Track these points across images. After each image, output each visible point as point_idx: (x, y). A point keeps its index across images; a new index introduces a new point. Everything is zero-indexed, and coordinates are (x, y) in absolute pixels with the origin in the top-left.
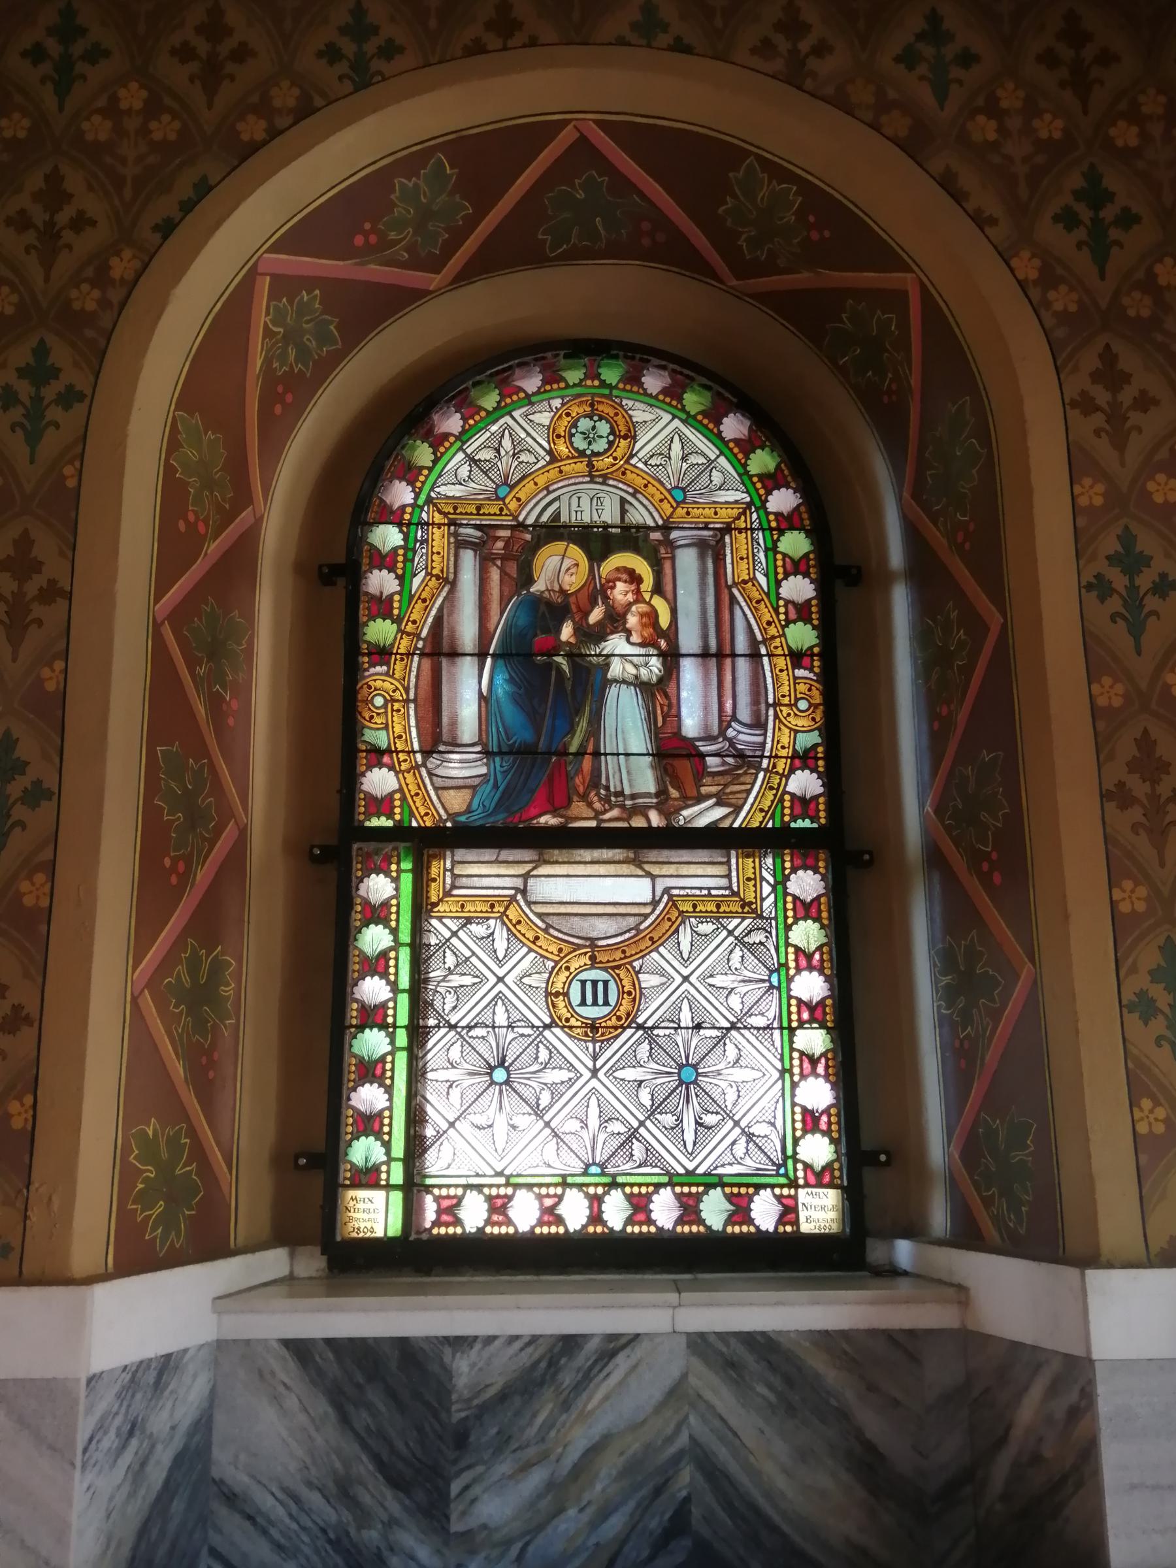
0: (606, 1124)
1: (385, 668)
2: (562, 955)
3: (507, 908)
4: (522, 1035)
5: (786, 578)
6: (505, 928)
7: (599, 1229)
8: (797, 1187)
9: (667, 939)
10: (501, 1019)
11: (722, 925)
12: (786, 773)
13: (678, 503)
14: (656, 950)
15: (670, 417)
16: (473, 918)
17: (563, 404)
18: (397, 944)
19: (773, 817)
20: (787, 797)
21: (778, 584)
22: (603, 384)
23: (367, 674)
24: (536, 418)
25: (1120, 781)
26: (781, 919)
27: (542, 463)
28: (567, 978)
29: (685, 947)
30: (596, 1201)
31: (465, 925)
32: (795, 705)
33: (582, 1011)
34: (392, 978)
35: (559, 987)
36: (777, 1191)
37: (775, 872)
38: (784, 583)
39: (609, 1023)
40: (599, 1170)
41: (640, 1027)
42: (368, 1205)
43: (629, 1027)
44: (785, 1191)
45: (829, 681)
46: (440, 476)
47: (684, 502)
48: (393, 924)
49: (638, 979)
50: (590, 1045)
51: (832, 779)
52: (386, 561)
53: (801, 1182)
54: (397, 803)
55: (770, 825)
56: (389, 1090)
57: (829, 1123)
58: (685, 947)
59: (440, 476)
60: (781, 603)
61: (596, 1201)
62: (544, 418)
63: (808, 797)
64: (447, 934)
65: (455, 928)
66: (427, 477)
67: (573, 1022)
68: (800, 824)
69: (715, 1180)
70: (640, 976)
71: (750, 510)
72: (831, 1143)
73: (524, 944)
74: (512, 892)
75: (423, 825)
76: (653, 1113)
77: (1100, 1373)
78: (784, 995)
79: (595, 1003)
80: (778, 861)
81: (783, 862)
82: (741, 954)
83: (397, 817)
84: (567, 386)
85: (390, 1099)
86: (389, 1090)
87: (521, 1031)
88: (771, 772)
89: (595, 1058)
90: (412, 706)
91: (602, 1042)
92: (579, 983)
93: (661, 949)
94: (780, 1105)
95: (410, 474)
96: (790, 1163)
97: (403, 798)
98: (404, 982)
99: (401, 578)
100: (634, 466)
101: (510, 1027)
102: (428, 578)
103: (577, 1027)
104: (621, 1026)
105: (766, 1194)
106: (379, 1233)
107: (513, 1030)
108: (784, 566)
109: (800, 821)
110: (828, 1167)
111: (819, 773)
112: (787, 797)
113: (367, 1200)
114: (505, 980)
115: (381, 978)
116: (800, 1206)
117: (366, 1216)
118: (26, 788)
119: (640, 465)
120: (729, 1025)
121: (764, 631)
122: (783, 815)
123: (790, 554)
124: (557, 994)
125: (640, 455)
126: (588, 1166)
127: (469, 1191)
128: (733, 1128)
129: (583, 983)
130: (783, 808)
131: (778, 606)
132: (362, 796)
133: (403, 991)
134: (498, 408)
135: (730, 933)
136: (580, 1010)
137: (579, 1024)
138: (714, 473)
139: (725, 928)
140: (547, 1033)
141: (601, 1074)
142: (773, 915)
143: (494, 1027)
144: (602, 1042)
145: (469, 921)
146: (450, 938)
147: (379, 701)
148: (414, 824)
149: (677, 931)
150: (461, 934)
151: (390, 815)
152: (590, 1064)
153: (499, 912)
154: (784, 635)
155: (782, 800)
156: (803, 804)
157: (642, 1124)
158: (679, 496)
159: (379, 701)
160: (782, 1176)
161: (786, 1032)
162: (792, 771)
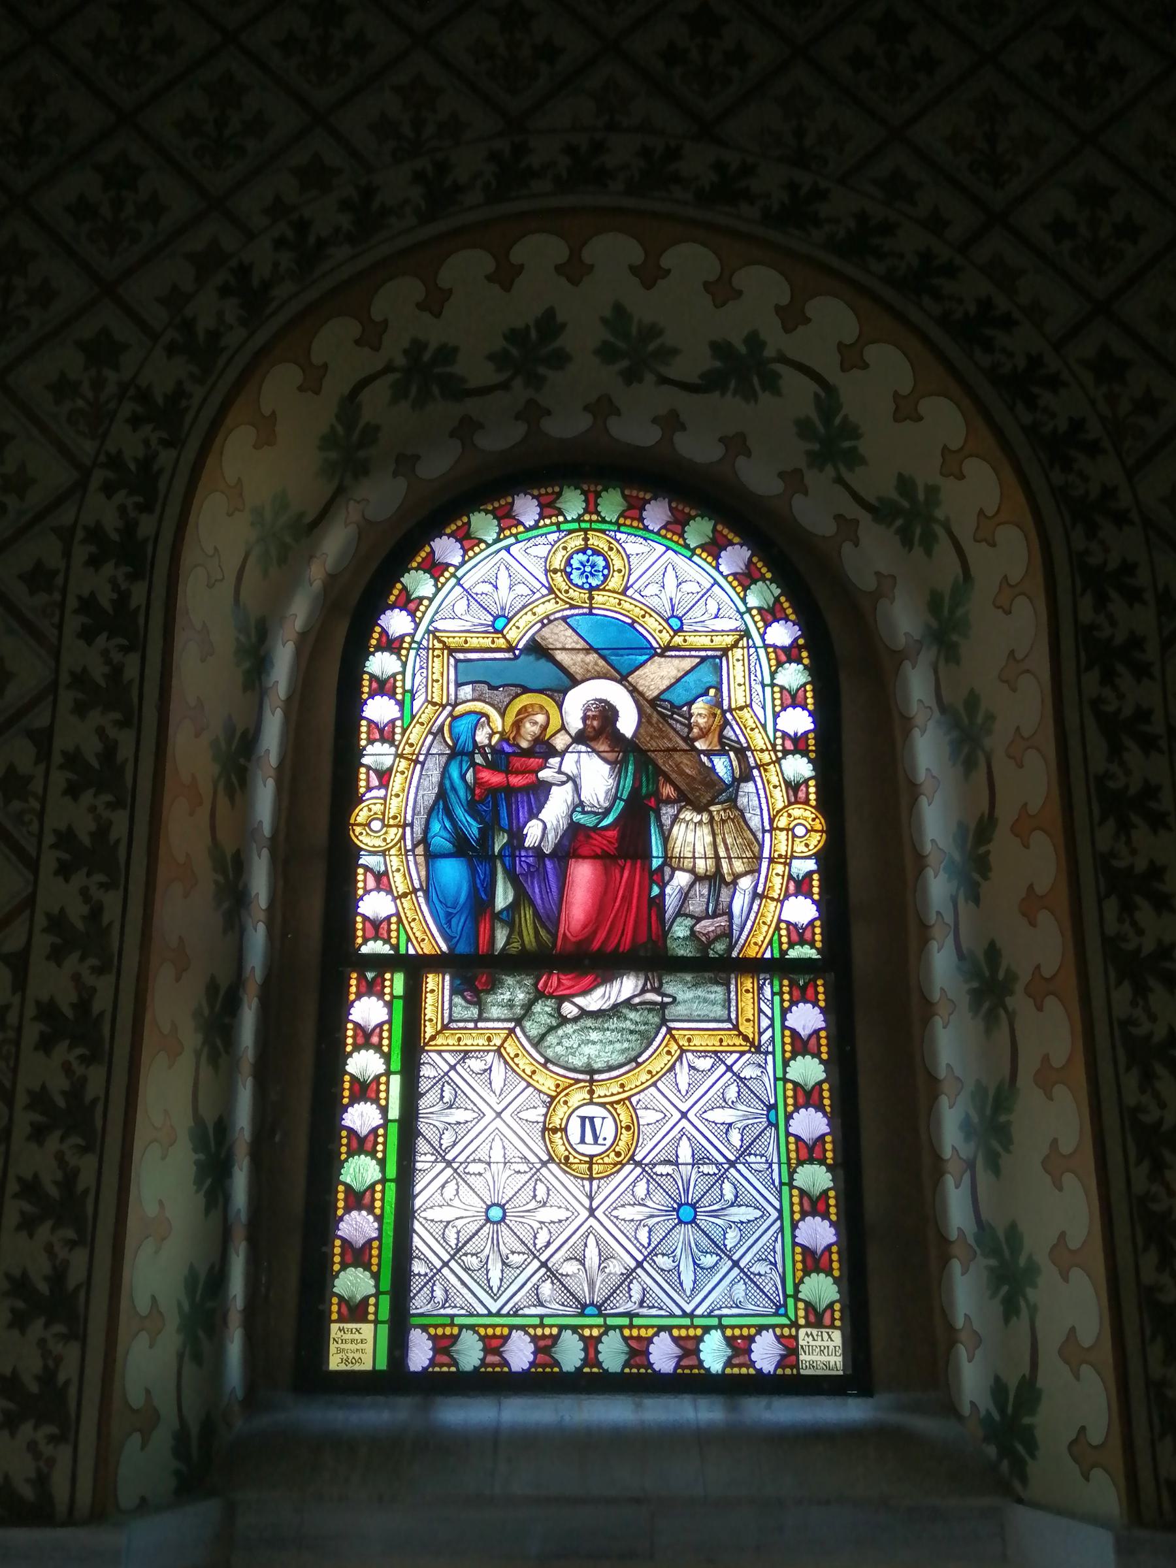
3: (505, 1040)
4: (519, 1172)
5: (802, 1219)
10: (497, 1155)
11: (720, 1059)
12: (781, 898)
16: (471, 1051)
18: (388, 1073)
20: (783, 925)
27: (538, 595)
34: (383, 1102)
35: (556, 1122)
37: (772, 1004)
41: (638, 1164)
42: (357, 1336)
43: (628, 1163)
47: (681, 629)
48: (375, 1268)
50: (587, 1183)
54: (394, 927)
55: (768, 955)
60: (779, 734)
62: (543, 551)
64: (446, 1068)
66: (427, 607)
69: (715, 1322)
73: (523, 1079)
75: (420, 952)
91: (599, 1179)
92: (579, 1120)
95: (409, 604)
96: (791, 1301)
98: (394, 1113)
99: (401, 704)
100: (631, 597)
104: (620, 1163)
106: (367, 1366)
108: (789, 936)
111: (820, 1008)
112: (783, 925)
113: (354, 1330)
115: (365, 1270)
117: (354, 1347)
119: (637, 596)
123: (787, 687)
124: (555, 1131)
125: (636, 586)
129: (583, 1119)
132: (344, 1133)
133: (390, 1181)
139: (724, 1063)
143: (489, 1164)
145: (466, 1054)
146: (449, 1071)
148: (411, 951)
149: (672, 1068)
152: (586, 1202)
153: (495, 1045)
154: (782, 903)
156: (799, 934)
158: (675, 623)
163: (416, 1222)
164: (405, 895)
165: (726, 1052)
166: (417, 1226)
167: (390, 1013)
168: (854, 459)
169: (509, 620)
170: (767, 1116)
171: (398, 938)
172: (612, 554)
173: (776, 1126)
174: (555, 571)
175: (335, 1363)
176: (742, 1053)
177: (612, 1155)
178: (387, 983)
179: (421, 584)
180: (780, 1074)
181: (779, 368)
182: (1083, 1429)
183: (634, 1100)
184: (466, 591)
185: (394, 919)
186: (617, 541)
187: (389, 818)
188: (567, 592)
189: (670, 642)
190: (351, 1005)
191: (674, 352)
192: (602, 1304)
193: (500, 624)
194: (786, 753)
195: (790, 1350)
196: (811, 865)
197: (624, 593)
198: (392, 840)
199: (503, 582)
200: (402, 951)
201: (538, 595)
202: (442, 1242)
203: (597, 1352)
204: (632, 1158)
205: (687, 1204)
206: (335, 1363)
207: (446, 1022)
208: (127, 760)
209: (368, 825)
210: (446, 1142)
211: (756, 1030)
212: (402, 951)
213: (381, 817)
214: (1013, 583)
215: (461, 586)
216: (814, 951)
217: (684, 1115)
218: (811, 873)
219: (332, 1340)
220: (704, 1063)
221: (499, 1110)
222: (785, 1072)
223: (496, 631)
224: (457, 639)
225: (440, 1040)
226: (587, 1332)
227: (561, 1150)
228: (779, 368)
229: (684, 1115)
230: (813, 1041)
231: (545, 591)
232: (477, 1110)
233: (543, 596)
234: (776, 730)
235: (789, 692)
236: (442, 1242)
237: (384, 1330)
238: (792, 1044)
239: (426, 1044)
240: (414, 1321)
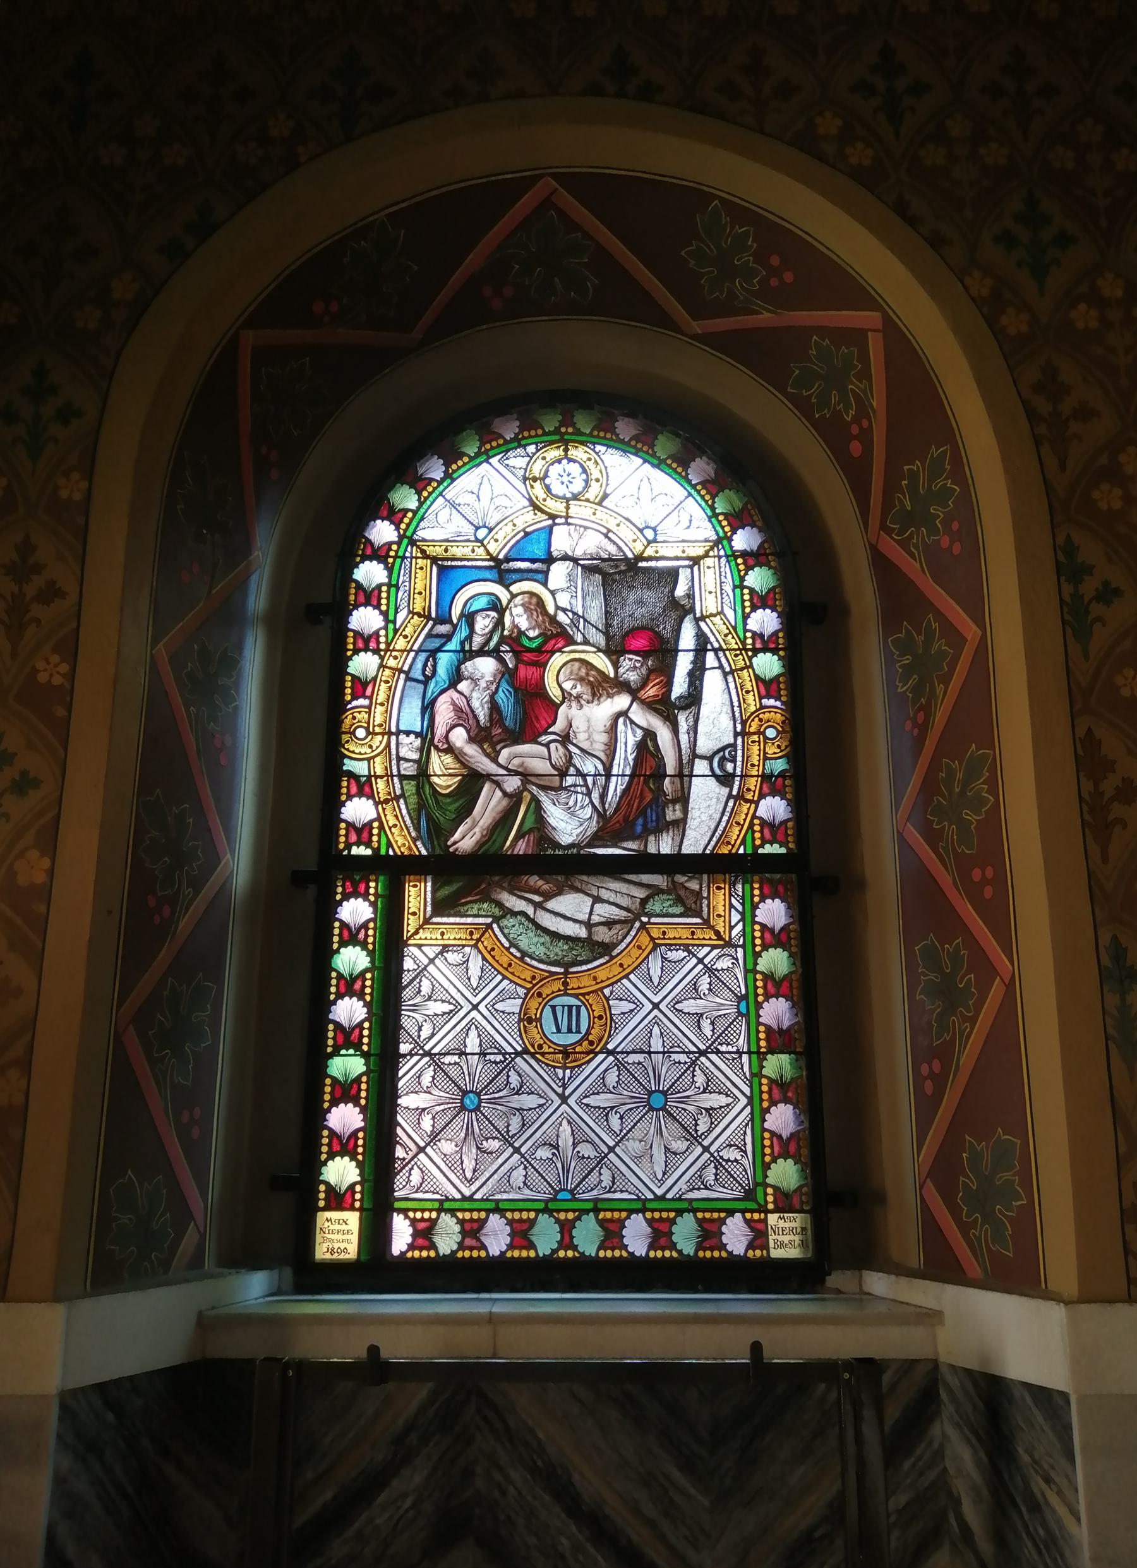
0: (458, 1149)
2: (534, 982)
6: (480, 956)
7: (570, 1254)
9: (493, 967)
13: (649, 542)
14: (627, 977)
21: (746, 617)
23: (349, 706)
24: (511, 462)
25: (1130, 805)
28: (540, 1004)
29: (655, 973)
30: (566, 1228)
36: (748, 1215)
40: (569, 1197)
43: (601, 1052)
44: (756, 1216)
47: (655, 541)
49: (608, 1004)
51: (798, 805)
52: (370, 597)
53: (771, 1206)
54: (375, 831)
55: (741, 851)
57: (799, 1147)
58: (655, 973)
60: (749, 635)
61: (566, 1228)
63: (777, 822)
67: (545, 1049)
68: (768, 849)
69: (685, 1205)
71: (718, 548)
72: (357, 1166)
74: (489, 920)
77: (72, 1385)
79: (570, 1031)
80: (747, 887)
81: (752, 889)
82: (708, 980)
84: (545, 434)
87: (492, 1058)
91: (573, 1068)
93: (632, 977)
94: (749, 1131)
97: (381, 827)
99: (385, 614)
101: (482, 1054)
102: (411, 615)
103: (549, 1053)
104: (592, 1051)
107: (738, 1050)
109: (767, 846)
113: (341, 1221)
114: (471, 1007)
117: (340, 1237)
118: (1118, 786)
126: (557, 1192)
127: (541, 1214)
128: (512, 1155)
130: (754, 832)
131: (745, 638)
134: (478, 455)
135: (700, 961)
137: (551, 1050)
139: (694, 955)
140: (518, 1060)
141: (571, 1101)
142: (741, 942)
143: (649, 1053)
144: (573, 1068)
151: (368, 844)
154: (751, 666)
156: (772, 830)
157: (706, 1149)
158: (649, 534)
161: (754, 1057)
163: (398, 1116)
164: (386, 801)
165: (698, 946)
166: (399, 1118)
169: (491, 530)
170: (738, 1006)
171: (379, 842)
172: (591, 464)
175: (322, 1253)
177: (585, 1043)
179: (405, 498)
180: (750, 966)
183: (607, 992)
184: (449, 501)
187: (374, 726)
189: (644, 551)
190: (343, 804)
193: (481, 533)
194: (756, 652)
197: (600, 504)
198: (377, 747)
199: (485, 494)
200: (383, 852)
202: (435, 982)
203: (572, 1237)
205: (658, 1091)
206: (322, 1253)
207: (428, 915)
209: (353, 733)
210: (425, 1033)
211: (727, 924)
213: (366, 725)
215: (444, 497)
217: (656, 1006)
219: (318, 1230)
221: (475, 1003)
222: (756, 964)
223: (477, 540)
224: (437, 548)
225: (421, 934)
226: (562, 1216)
229: (656, 1006)
232: (454, 1002)
234: (745, 631)
236: (435, 982)
239: (408, 939)
240: (397, 1205)
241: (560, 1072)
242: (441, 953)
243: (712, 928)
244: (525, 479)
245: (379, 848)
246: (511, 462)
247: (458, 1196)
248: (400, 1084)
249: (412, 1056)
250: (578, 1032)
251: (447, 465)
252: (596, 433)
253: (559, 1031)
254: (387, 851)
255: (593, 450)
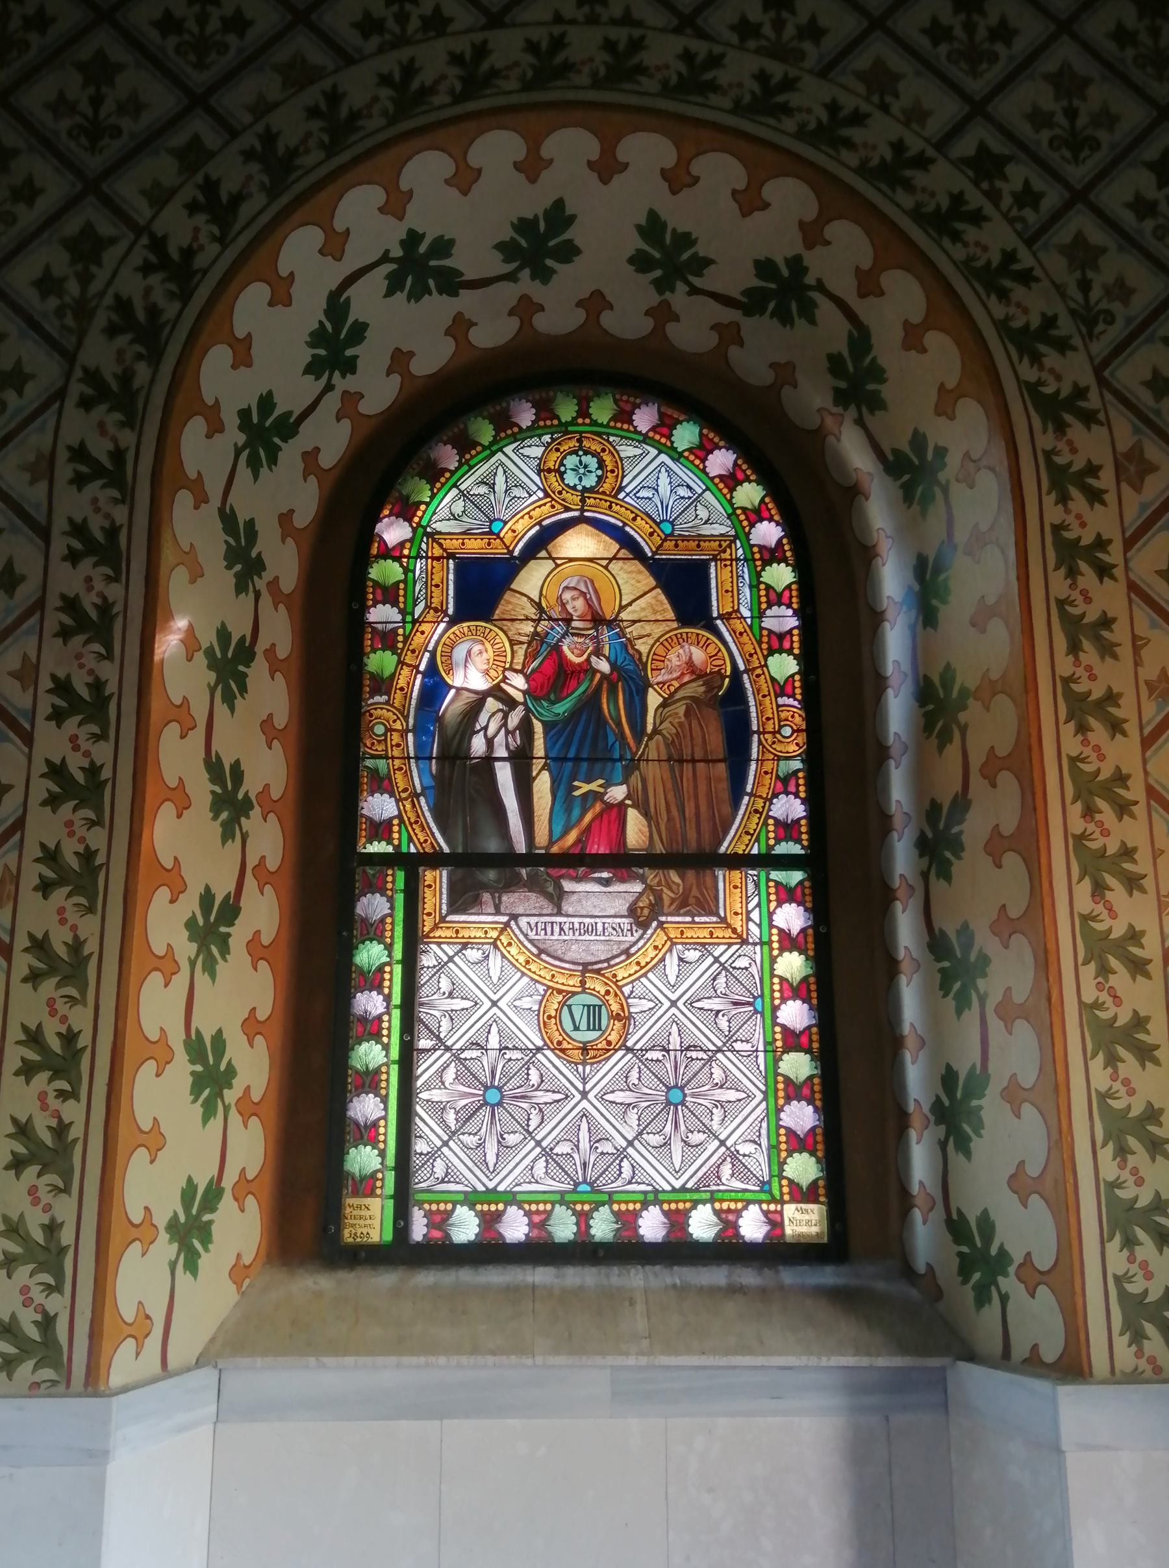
1: (385, 698)
8: (782, 1202)
14: (645, 975)
15: (656, 452)
17: (553, 440)
19: (757, 840)
20: (771, 821)
22: (595, 423)
24: (526, 451)
26: (767, 999)
27: (534, 498)
31: (460, 951)
32: (779, 732)
33: (576, 1035)
38: (779, 959)
39: (599, 1046)
41: (629, 1050)
43: (620, 1049)
44: (772, 1207)
45: (811, 704)
46: (434, 513)
51: (814, 803)
55: (755, 851)
56: (385, 1100)
59: (434, 513)
62: (537, 452)
65: (451, 953)
67: (565, 1045)
70: (630, 1001)
73: (519, 970)
76: (641, 1134)
78: (768, 1021)
83: (396, 842)
85: (386, 1109)
86: (385, 1100)
88: (756, 796)
89: (584, 1081)
90: (410, 736)
94: (764, 1125)
96: (775, 1180)
98: (397, 999)
105: (754, 1209)
106: (375, 1238)
110: (814, 1185)
112: (771, 821)
116: (786, 1222)
120: (714, 1048)
121: (747, 662)
122: (768, 839)
125: (628, 490)
128: (450, 1149)
131: (761, 636)
136: (574, 1035)
138: (737, 964)
139: (711, 954)
145: (465, 946)
147: (379, 729)
148: (413, 850)
149: (663, 959)
150: (456, 959)
152: (580, 1087)
154: (766, 665)
155: (766, 824)
158: (667, 528)
159: (379, 729)
160: (764, 1192)
162: (776, 795)
166: (418, 1109)
167: (392, 908)
168: (876, 403)
171: (400, 839)
173: (762, 1014)
174: (549, 471)
176: (730, 945)
178: (389, 879)
181: (816, 296)
182: (1022, 1164)
185: (396, 822)
186: (610, 443)
188: (560, 493)
191: (708, 262)
192: (595, 1181)
195: (775, 1222)
196: (797, 765)
201: (534, 498)
204: (624, 1045)
206: (347, 1236)
208: (113, 694)
212: (404, 850)
214: (974, 457)
216: (798, 847)
218: (798, 770)
220: (692, 955)
227: (557, 1037)
228: (816, 296)
230: (799, 891)
231: (541, 494)
233: (540, 499)
235: (791, 985)
237: (390, 1203)
238: (776, 893)
241: (580, 1068)
242: (460, 951)
243: (729, 926)
244: (539, 472)
245: (399, 846)
246: (526, 451)
247: (668, 1188)
248: (419, 1083)
249: (435, 1050)
250: (600, 1029)
251: (461, 454)
252: (612, 424)
253: (576, 1028)
254: (409, 847)
255: (608, 441)
